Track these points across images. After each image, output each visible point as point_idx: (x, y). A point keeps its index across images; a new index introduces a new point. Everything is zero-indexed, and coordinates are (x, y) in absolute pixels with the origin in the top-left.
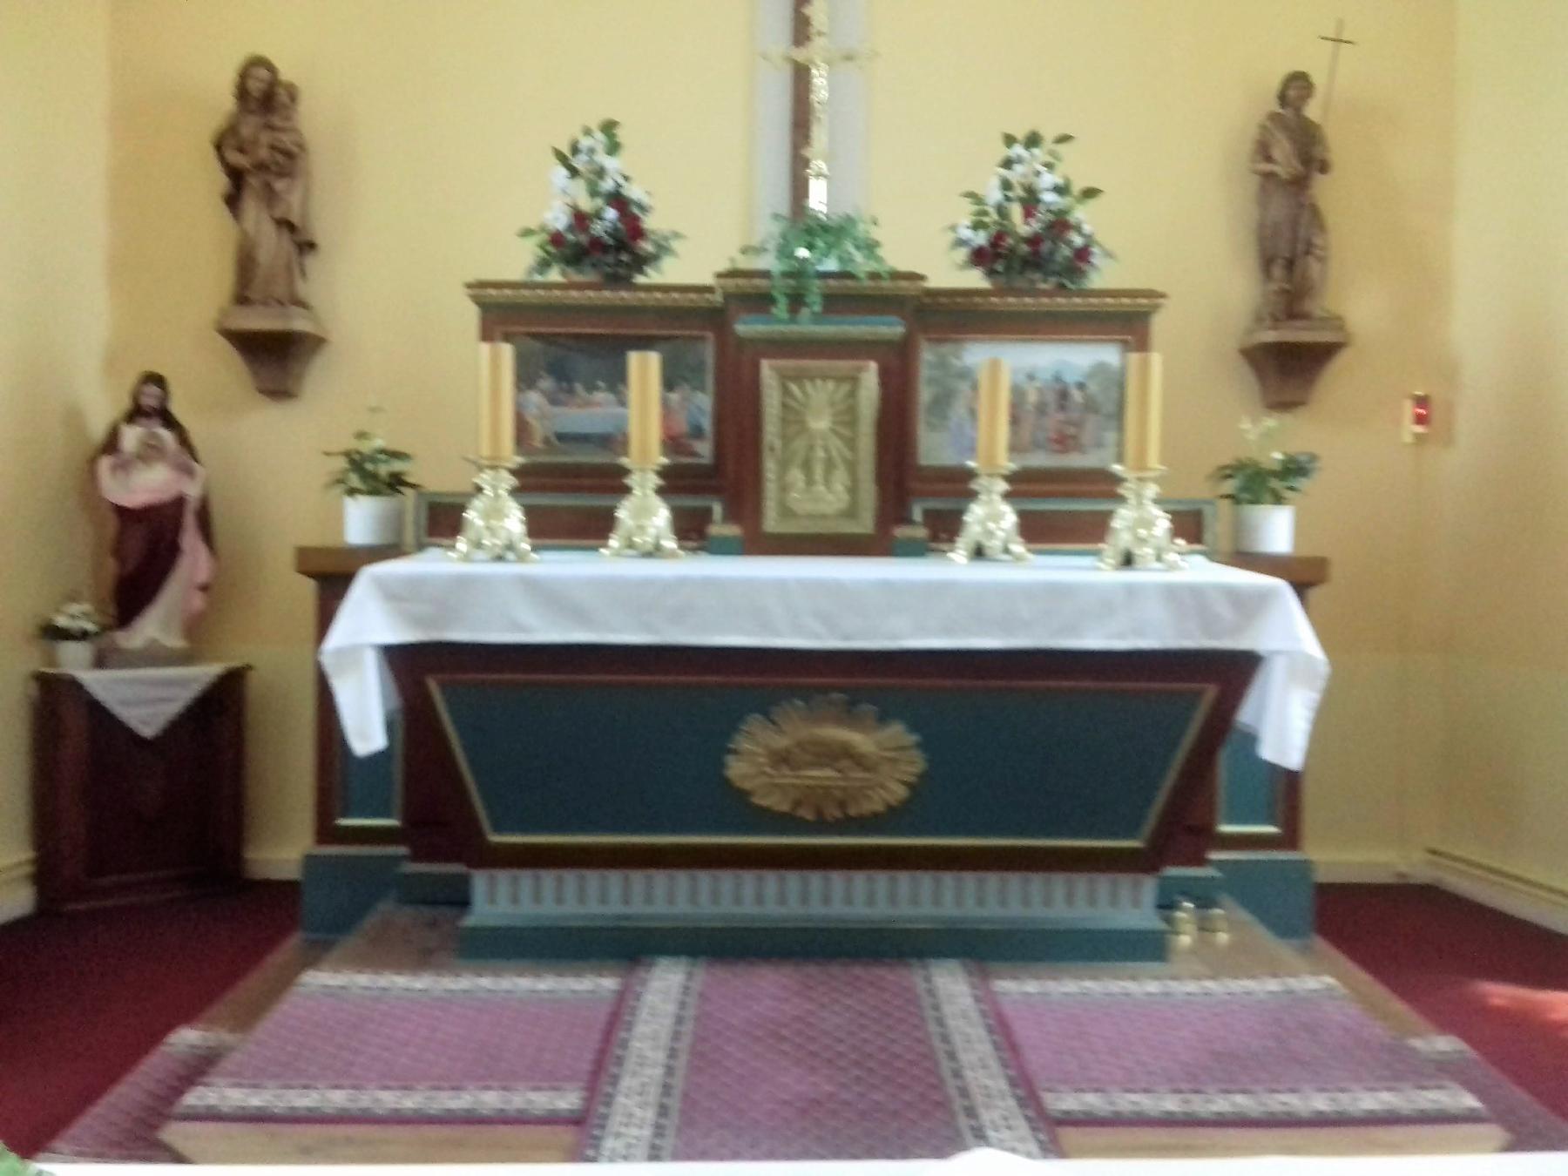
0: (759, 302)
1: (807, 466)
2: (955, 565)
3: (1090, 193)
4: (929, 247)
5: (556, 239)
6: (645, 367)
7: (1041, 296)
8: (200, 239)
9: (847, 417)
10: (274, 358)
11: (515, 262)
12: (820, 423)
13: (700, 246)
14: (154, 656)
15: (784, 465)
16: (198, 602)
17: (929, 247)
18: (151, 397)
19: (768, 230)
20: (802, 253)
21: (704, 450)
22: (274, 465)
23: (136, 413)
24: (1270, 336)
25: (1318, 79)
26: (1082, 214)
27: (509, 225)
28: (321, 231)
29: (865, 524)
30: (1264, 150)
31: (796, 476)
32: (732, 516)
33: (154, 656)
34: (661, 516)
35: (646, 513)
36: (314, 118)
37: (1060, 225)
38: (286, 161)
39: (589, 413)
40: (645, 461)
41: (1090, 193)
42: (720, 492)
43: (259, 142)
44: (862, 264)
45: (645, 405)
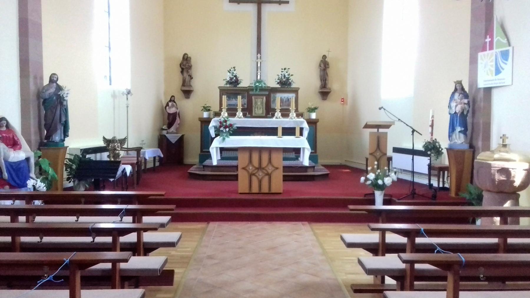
0: (252, 90)
1: (258, 108)
2: (274, 119)
3: (292, 75)
4: (272, 82)
5: (228, 81)
6: (239, 97)
7: (286, 88)
8: (177, 79)
9: (262, 103)
10: (187, 93)
11: (223, 84)
12: (259, 103)
13: (245, 83)
14: (172, 133)
15: (255, 108)
16: (178, 126)
17: (272, 82)
18: (173, 99)
19: (253, 82)
20: (257, 84)
21: (246, 106)
22: (190, 109)
23: (170, 101)
24: (321, 91)
25: (327, 56)
26: (291, 78)
27: (222, 79)
28: (193, 76)
29: (264, 115)
30: (320, 66)
31: (256, 109)
32: (249, 114)
33: (172, 133)
34: (241, 114)
35: (240, 114)
36: (193, 62)
37: (288, 79)
38: (190, 67)
39: (233, 102)
40: (240, 107)
41: (292, 75)
42: (248, 111)
43: (186, 65)
44: (264, 85)
45: (240, 101)
